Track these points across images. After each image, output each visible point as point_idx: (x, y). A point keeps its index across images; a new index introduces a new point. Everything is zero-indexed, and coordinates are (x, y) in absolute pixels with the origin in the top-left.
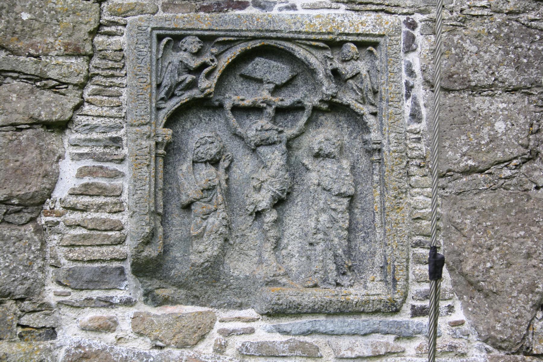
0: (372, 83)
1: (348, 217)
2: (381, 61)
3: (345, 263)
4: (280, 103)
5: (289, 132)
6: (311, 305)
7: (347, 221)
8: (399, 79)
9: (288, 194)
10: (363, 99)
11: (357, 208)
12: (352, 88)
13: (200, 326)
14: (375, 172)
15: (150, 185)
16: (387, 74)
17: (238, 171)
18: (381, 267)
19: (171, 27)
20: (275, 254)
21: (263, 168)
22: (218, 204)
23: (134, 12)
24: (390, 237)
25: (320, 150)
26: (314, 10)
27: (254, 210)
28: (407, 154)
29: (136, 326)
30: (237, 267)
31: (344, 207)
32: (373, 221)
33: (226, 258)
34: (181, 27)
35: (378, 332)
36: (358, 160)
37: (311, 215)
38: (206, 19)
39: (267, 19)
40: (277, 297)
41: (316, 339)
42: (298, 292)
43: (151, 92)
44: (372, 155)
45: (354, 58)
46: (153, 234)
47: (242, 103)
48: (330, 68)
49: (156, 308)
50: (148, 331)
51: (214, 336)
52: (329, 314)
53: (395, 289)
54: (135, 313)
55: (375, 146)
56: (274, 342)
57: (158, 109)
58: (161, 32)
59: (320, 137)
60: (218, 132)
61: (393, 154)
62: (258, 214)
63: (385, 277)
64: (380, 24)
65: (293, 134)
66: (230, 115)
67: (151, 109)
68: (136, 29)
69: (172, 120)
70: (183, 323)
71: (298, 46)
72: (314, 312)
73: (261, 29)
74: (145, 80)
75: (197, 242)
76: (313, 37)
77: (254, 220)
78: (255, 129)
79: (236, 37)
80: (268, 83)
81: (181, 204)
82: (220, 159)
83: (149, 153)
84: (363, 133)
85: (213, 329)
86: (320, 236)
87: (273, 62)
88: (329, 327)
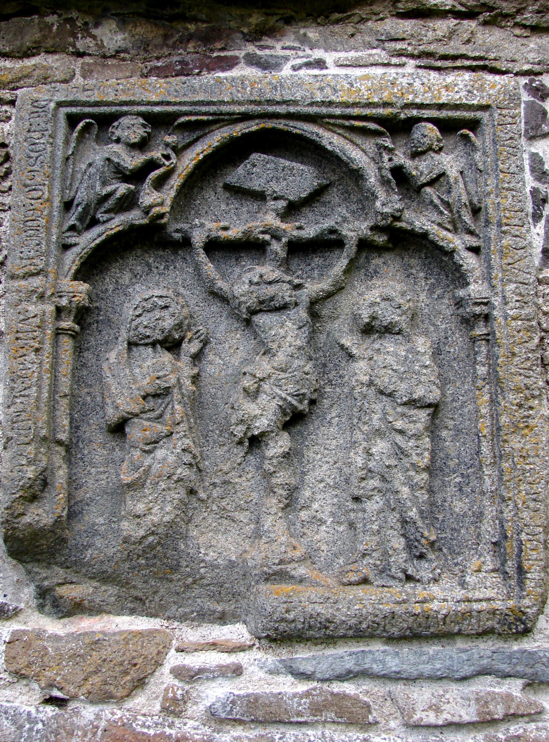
0: (468, 193)
1: (428, 446)
2: (484, 153)
3: (422, 536)
4: (295, 233)
5: (314, 287)
6: (353, 621)
7: (426, 454)
8: (520, 185)
9: (313, 402)
10: (453, 222)
11: (446, 427)
12: (432, 202)
13: (135, 661)
14: (479, 359)
15: (40, 387)
16: (497, 175)
17: (218, 361)
18: (495, 544)
19: (92, 99)
20: (286, 518)
21: (264, 354)
22: (174, 423)
23: (31, 81)
24: (511, 484)
25: (373, 318)
26: (358, 69)
27: (245, 434)
28: (539, 324)
29: (14, 658)
30: (214, 543)
31: (420, 426)
32: (478, 453)
33: (191, 527)
34: (111, 99)
35: (489, 674)
36: (446, 338)
37: (355, 442)
38: (158, 86)
39: (270, 83)
40: (285, 606)
41: (364, 687)
42: (327, 595)
43: (50, 215)
44: (472, 328)
45: (434, 147)
46: (44, 482)
47: (223, 234)
48: (387, 165)
49: (62, 621)
50: (36, 668)
51: (164, 680)
52: (391, 639)
53: (522, 590)
54: (14, 633)
55: (478, 310)
56: (280, 694)
57: (66, 247)
58: (74, 110)
59: (374, 295)
60: (182, 290)
61: (513, 323)
62: (255, 442)
63: (503, 564)
64: (481, 89)
65: (323, 291)
66: (202, 257)
67: (48, 245)
68: (30, 106)
69: (93, 266)
70: (104, 654)
71: (329, 130)
72: (360, 633)
73: (258, 99)
74: (40, 193)
75: (132, 496)
76: (356, 111)
77: (246, 453)
78: (247, 281)
79: (211, 114)
80: (276, 199)
81: (107, 424)
82: (182, 339)
83: (39, 327)
84: (456, 288)
85: (161, 665)
86: (374, 483)
87: (282, 161)
88: (390, 664)
